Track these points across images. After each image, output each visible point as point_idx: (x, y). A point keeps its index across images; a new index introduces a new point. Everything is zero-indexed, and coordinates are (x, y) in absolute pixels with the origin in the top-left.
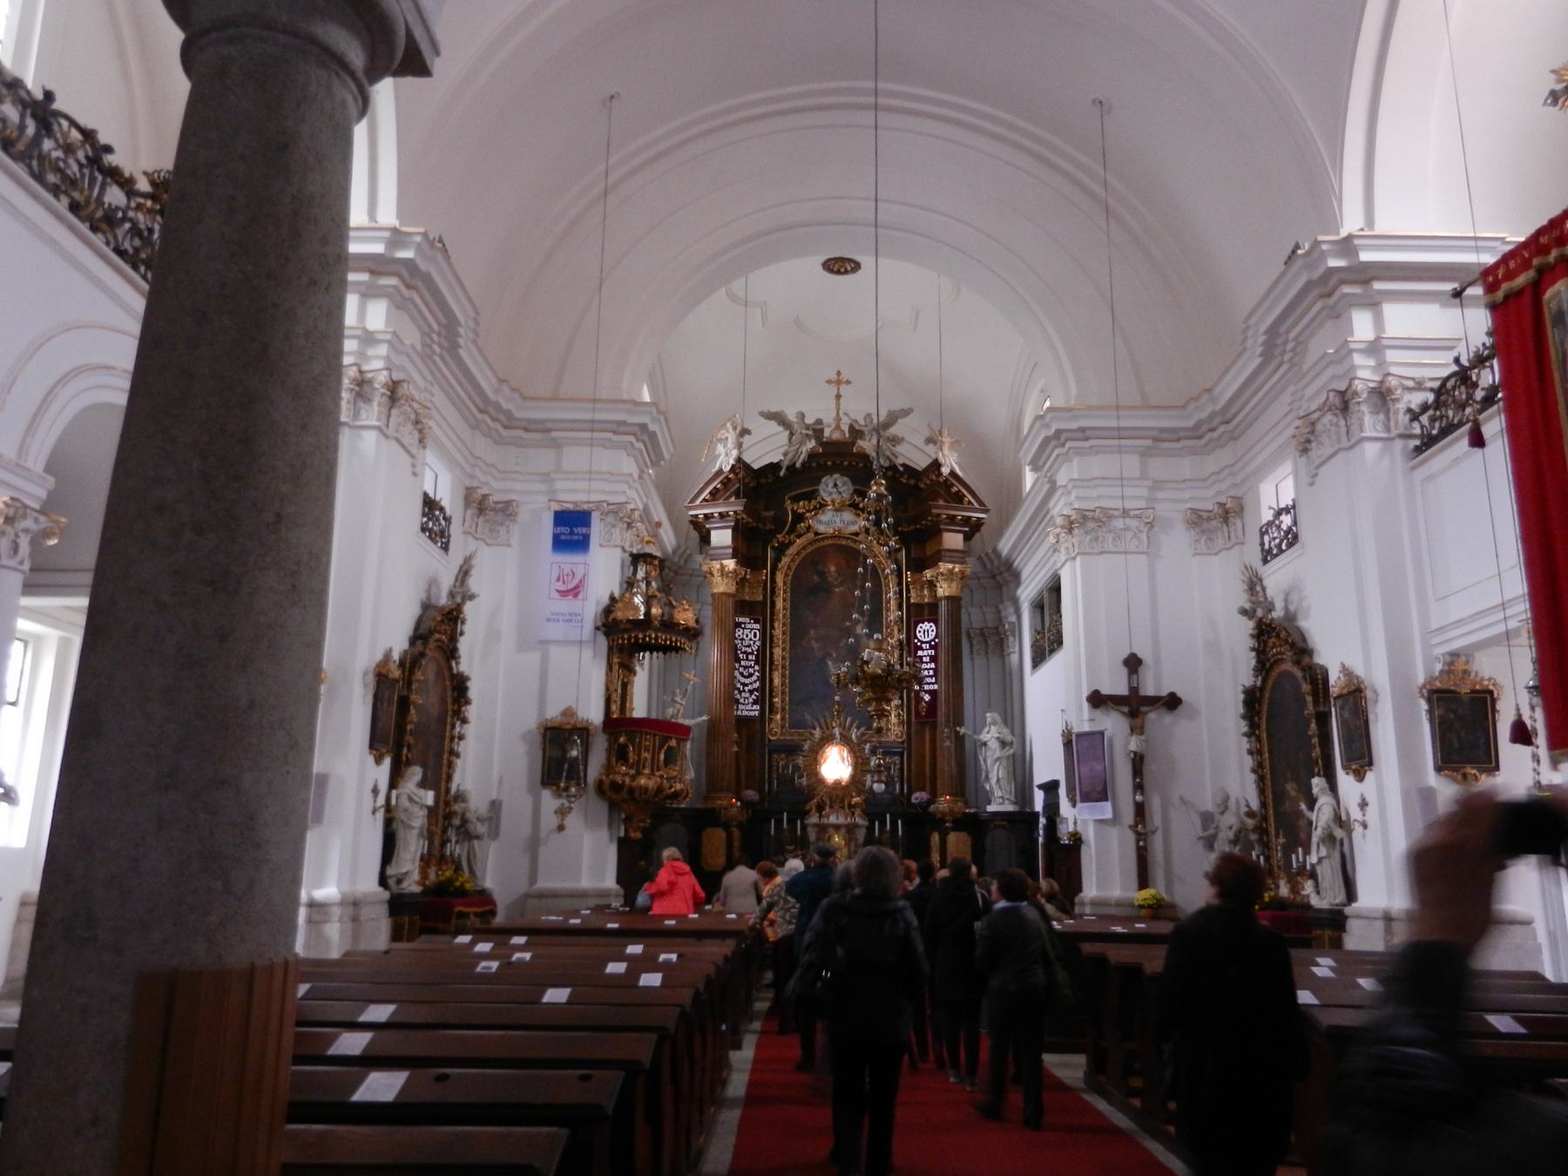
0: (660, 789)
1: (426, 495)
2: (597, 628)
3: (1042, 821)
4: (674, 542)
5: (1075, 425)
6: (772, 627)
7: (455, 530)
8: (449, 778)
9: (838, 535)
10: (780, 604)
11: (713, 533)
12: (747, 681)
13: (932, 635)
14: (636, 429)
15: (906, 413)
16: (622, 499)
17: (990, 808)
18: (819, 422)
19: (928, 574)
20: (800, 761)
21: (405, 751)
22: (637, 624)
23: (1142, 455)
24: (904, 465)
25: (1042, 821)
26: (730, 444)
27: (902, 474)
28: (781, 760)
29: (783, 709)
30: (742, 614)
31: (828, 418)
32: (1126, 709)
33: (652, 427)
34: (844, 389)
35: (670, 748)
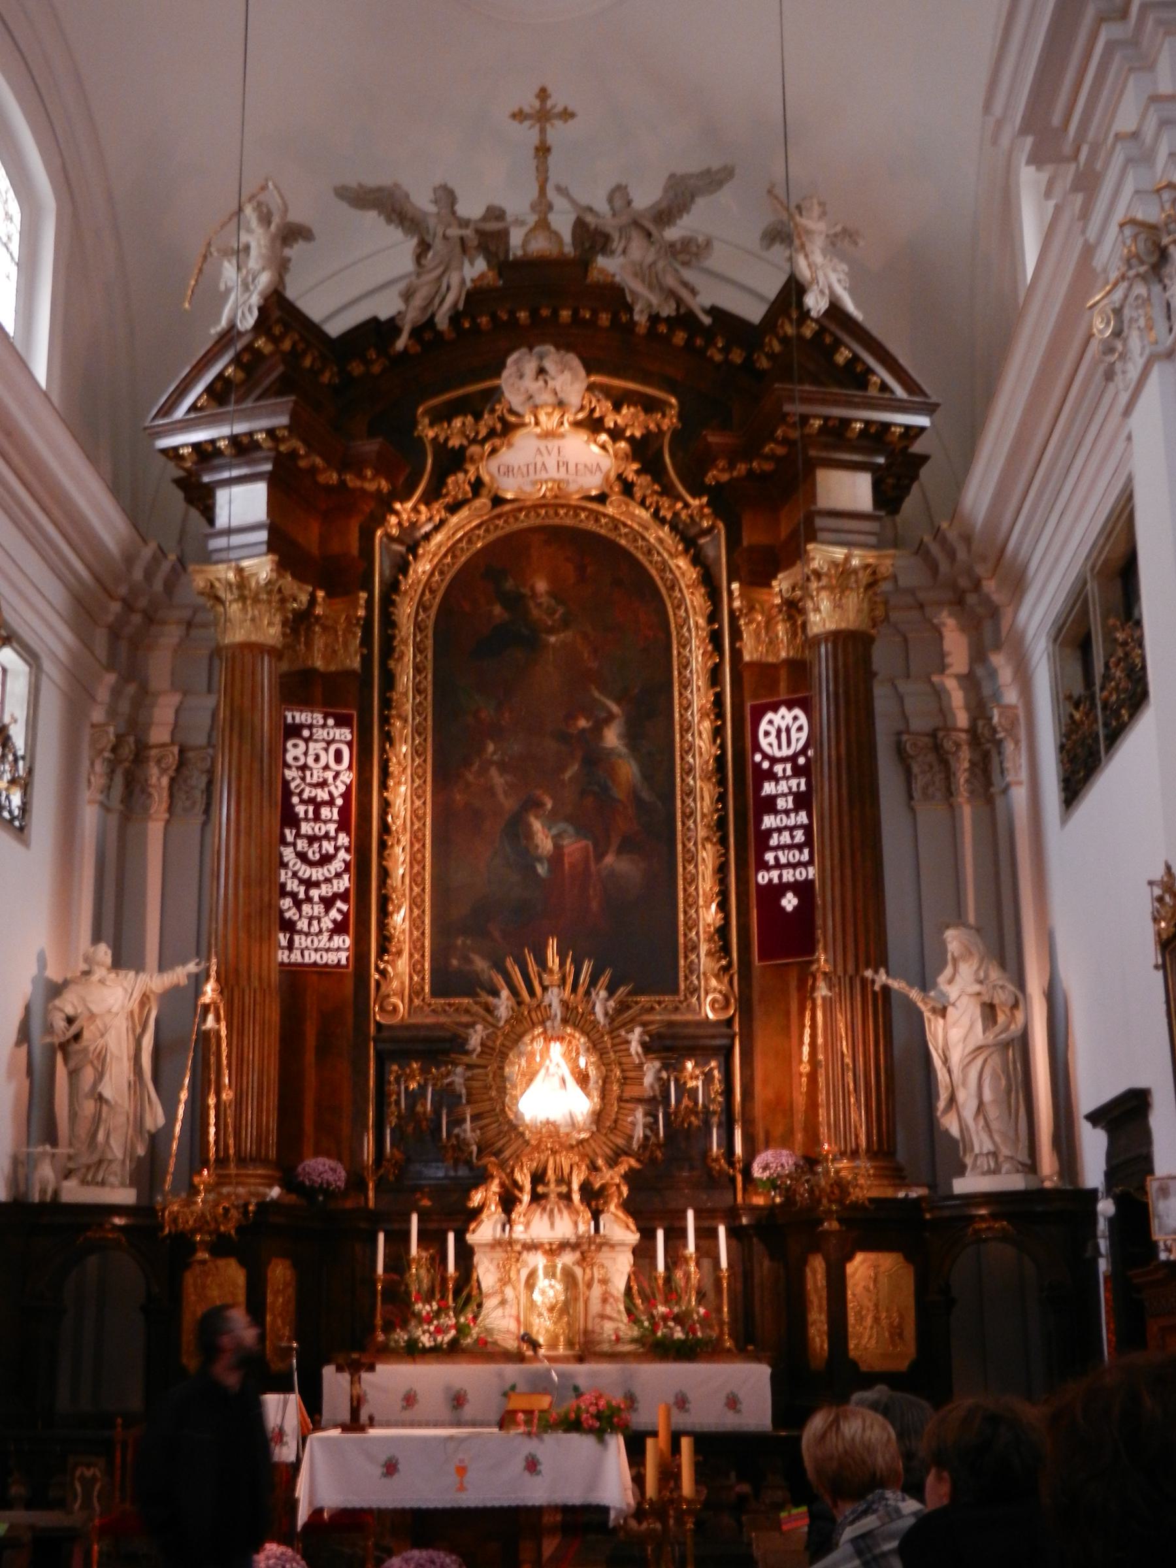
3: (1106, 1207)
10: (405, 679)
12: (317, 874)
13: (800, 739)
15: (714, 180)
17: (961, 1186)
18: (495, 213)
19: (782, 584)
20: (458, 1077)
24: (714, 311)
25: (1106, 1207)
26: (254, 262)
27: (709, 334)
28: (410, 1080)
30: (306, 703)
31: (518, 204)
34: (557, 133)
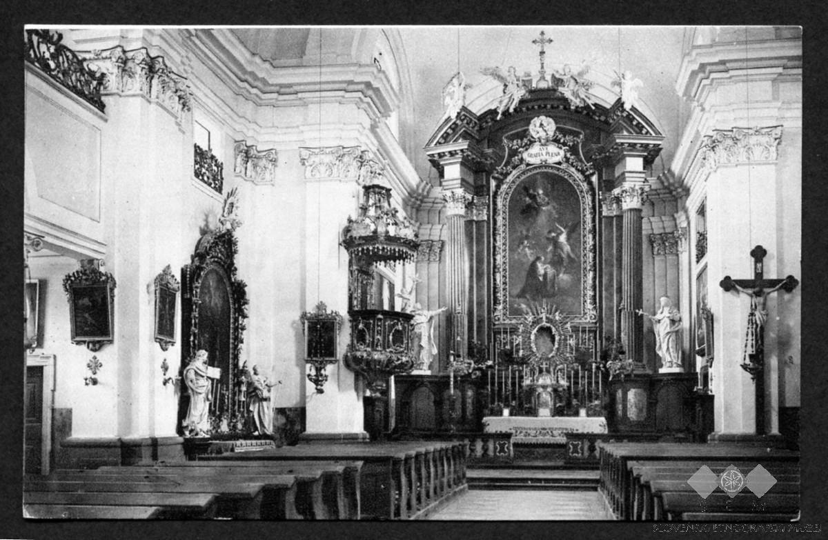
0: (390, 361)
1: (196, 147)
2: (340, 244)
4: (418, 180)
5: (716, 60)
6: (495, 240)
7: (227, 173)
8: (236, 357)
9: (544, 165)
11: (446, 168)
14: (362, 87)
16: (353, 144)
17: (662, 371)
19: (616, 191)
21: (192, 339)
22: (367, 240)
23: (774, 81)
24: (595, 105)
27: (594, 113)
29: (505, 301)
32: (750, 291)
33: (375, 84)
34: (547, 47)
35: (397, 331)
